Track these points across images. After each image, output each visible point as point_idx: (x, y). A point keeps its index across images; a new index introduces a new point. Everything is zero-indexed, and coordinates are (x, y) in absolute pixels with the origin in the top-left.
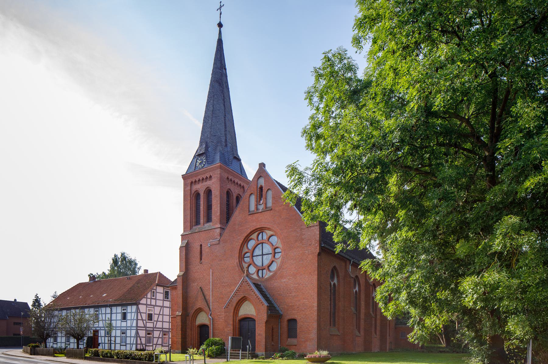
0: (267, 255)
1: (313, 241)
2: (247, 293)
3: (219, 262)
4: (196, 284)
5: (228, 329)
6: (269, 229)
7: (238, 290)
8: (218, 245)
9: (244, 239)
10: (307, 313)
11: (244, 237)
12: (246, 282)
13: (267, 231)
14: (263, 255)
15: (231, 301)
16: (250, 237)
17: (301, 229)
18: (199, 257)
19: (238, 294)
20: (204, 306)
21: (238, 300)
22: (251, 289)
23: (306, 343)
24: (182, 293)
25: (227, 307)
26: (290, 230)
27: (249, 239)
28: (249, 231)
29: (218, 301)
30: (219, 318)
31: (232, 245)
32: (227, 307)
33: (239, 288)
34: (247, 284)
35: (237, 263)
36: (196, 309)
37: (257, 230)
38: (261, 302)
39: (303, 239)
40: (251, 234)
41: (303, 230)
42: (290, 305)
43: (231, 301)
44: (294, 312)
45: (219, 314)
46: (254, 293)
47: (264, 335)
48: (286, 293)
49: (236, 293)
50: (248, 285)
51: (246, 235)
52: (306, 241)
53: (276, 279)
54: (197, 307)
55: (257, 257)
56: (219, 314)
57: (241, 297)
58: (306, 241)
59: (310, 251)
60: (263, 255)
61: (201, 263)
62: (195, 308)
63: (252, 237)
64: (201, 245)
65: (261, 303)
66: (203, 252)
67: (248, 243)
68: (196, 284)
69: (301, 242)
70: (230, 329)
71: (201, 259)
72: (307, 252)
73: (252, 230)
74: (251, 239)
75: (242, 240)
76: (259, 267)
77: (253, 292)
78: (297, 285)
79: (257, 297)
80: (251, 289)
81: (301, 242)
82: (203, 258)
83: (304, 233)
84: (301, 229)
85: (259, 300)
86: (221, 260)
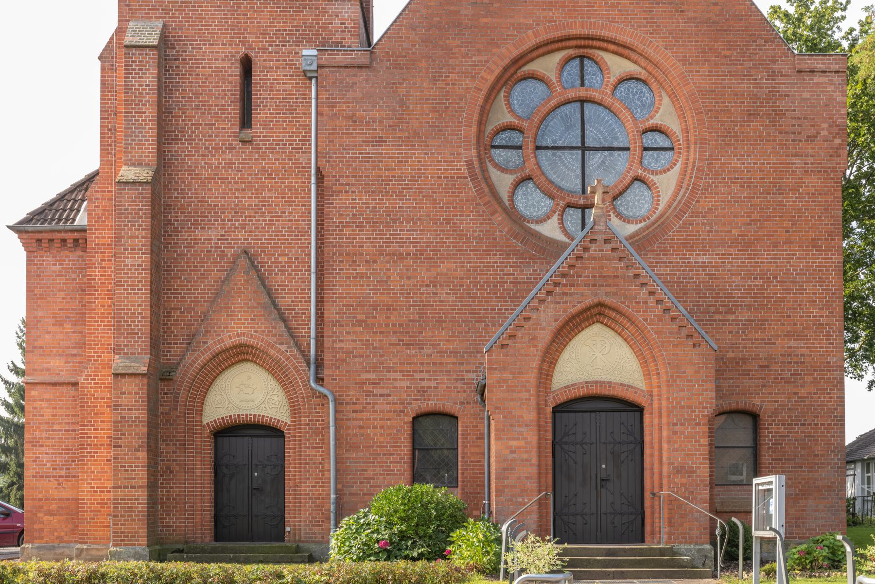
0: (606, 153)
1: (825, 125)
2: (612, 289)
3: (368, 149)
4: (213, 234)
5: (514, 443)
6: (622, 49)
7: (564, 275)
8: (364, 73)
9: (506, 69)
10: (803, 391)
11: (507, 61)
12: (606, 241)
13: (609, 59)
14: (584, 148)
15: (527, 319)
16: (524, 65)
17: (773, 75)
18: (234, 110)
19: (566, 289)
20: (272, 340)
21: (563, 318)
22: (636, 276)
23: (802, 502)
24: (147, 264)
25: (503, 346)
26: (726, 69)
27: (520, 73)
28: (531, 41)
29: (361, 317)
30: (368, 394)
31: (440, 84)
32: (503, 346)
33: (572, 266)
34: (614, 250)
35: (469, 164)
36: (218, 348)
37: (564, 44)
38: (684, 332)
39: (781, 113)
40: (535, 54)
41: (779, 80)
42: (731, 355)
43: (527, 319)
44: (746, 383)
45: (371, 376)
46: (652, 293)
47: (704, 471)
48: (713, 309)
49: (557, 284)
50: (616, 255)
51: (515, 53)
52: (794, 121)
53: (665, 251)
54: (228, 343)
55: (559, 153)
56: (371, 376)
57: (579, 307)
58: (794, 121)
59: (810, 160)
60: (584, 148)
61: (244, 142)
62: (213, 344)
63: (534, 67)
64: (247, 65)
65: (690, 336)
66: (259, 93)
67: (512, 87)
68: (213, 234)
69: (773, 123)
70: (522, 443)
71: (246, 121)
72: (797, 161)
73: (543, 37)
74: (532, 77)
75: (497, 71)
76: (570, 193)
77: (644, 290)
78: (760, 282)
79: (666, 310)
80: (636, 276)
81: (773, 123)
82: (259, 116)
83: (783, 89)
84: (773, 75)
85: (675, 326)
86: (381, 141)
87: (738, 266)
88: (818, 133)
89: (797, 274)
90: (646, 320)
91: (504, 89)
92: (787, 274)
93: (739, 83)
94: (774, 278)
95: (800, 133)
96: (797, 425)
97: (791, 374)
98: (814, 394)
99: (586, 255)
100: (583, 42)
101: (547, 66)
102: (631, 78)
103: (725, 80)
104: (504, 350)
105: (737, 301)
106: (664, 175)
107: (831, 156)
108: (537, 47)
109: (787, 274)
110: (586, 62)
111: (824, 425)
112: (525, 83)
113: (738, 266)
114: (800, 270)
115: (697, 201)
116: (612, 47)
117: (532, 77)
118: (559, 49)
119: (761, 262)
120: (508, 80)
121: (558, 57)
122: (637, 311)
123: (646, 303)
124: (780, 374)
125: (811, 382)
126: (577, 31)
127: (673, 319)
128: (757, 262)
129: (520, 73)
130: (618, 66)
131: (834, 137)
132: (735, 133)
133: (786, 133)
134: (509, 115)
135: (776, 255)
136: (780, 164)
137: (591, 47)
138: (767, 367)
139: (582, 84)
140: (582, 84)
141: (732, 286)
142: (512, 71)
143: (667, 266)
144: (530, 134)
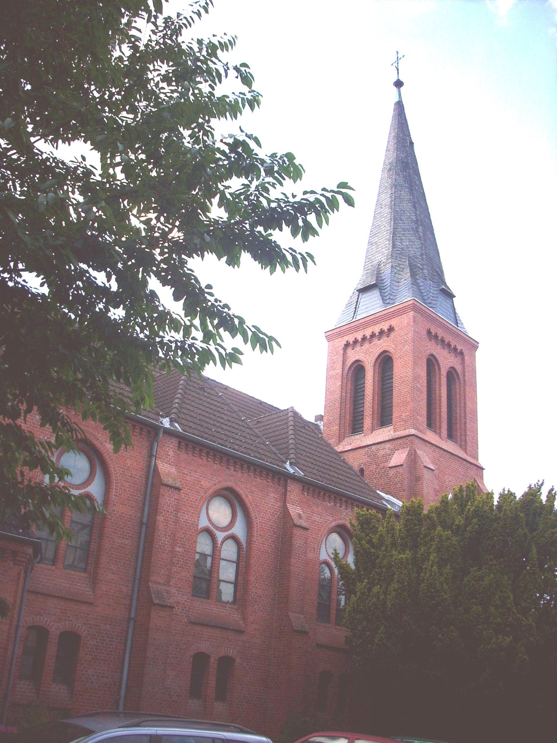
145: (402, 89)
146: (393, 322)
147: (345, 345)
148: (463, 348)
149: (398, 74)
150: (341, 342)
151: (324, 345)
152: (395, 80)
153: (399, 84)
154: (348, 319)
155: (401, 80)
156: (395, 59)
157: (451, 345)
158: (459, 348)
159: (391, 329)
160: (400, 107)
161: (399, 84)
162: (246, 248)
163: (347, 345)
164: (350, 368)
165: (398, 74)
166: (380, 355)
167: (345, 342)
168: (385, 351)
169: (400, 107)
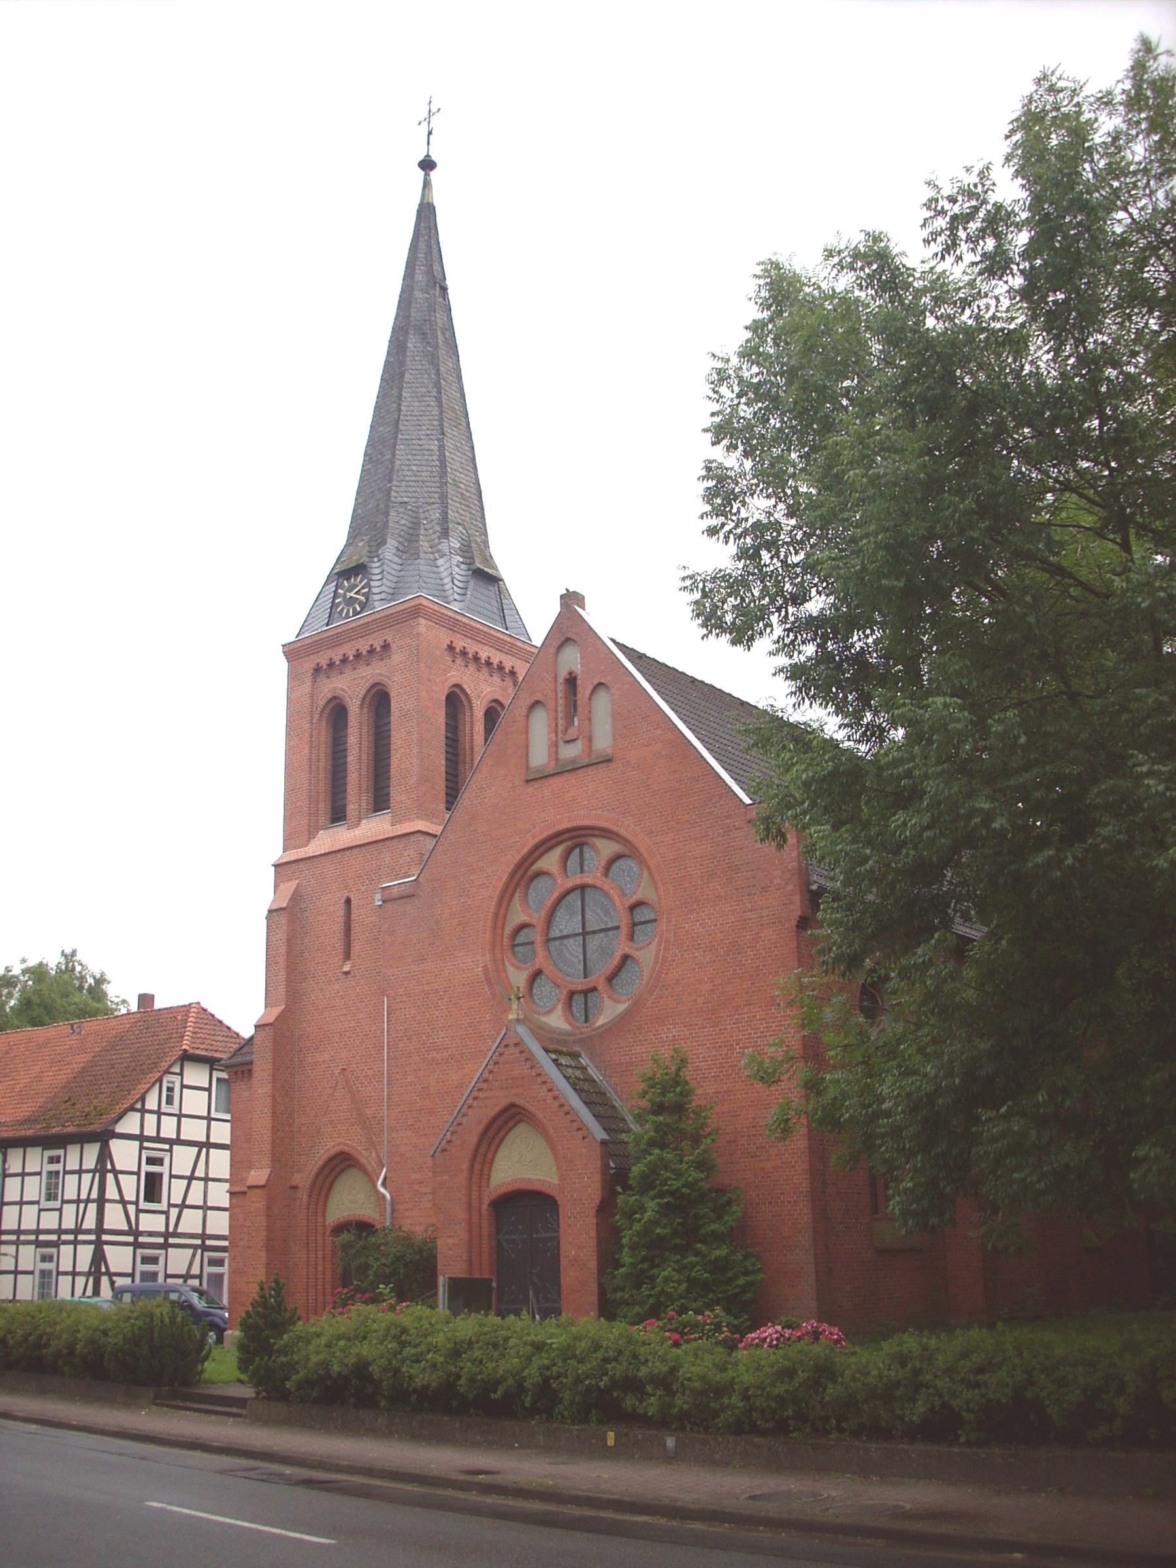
1: (777, 873)
4: (326, 1056)
9: (512, 875)
13: (599, 842)
16: (532, 864)
18: (339, 944)
32: (444, 1150)
35: (485, 968)
40: (537, 854)
59: (765, 912)
60: (585, 934)
64: (348, 901)
87: (705, 1036)
88: (771, 882)
89: (758, 1037)
90: (545, 1117)
91: (518, 890)
92: (749, 1038)
93: (698, 846)
94: (737, 1044)
95: (754, 886)
96: (765, 1204)
97: (757, 1148)
98: (780, 1167)
99: (501, 1060)
100: (574, 834)
101: (550, 861)
102: (618, 857)
103: (685, 845)
104: (445, 1154)
105: (704, 1074)
106: (646, 950)
107: (784, 904)
108: (537, 847)
109: (749, 1038)
110: (586, 849)
111: (789, 1202)
112: (535, 882)
113: (705, 1036)
114: (761, 1032)
115: (666, 974)
116: (597, 833)
117: (539, 874)
118: (558, 844)
119: (725, 1029)
120: (520, 880)
121: (557, 852)
122: (539, 1109)
123: (545, 1100)
124: (747, 1149)
125: (776, 1155)
126: (565, 825)
127: (567, 1113)
128: (721, 1030)
129: (530, 873)
130: (607, 848)
131: (787, 884)
132: (696, 897)
133: (742, 888)
134: (522, 914)
135: (737, 1019)
136: (738, 921)
137: (585, 836)
138: (734, 1142)
139: (582, 871)
140: (582, 871)
141: (699, 1058)
142: (520, 873)
143: (642, 1045)
144: (539, 929)
145: (432, 174)
146: (389, 636)
147: (314, 670)
148: (490, 655)
149: (428, 144)
150: (309, 665)
151: (283, 665)
152: (422, 158)
153: (427, 165)
154: (320, 626)
155: (434, 158)
156: (426, 115)
157: (480, 659)
158: (483, 655)
159: (386, 647)
160: (426, 214)
161: (427, 165)
162: (516, 646)
163: (317, 670)
164: (322, 712)
165: (428, 144)
166: (372, 687)
167: (313, 666)
168: (335, 698)
169: (426, 214)
